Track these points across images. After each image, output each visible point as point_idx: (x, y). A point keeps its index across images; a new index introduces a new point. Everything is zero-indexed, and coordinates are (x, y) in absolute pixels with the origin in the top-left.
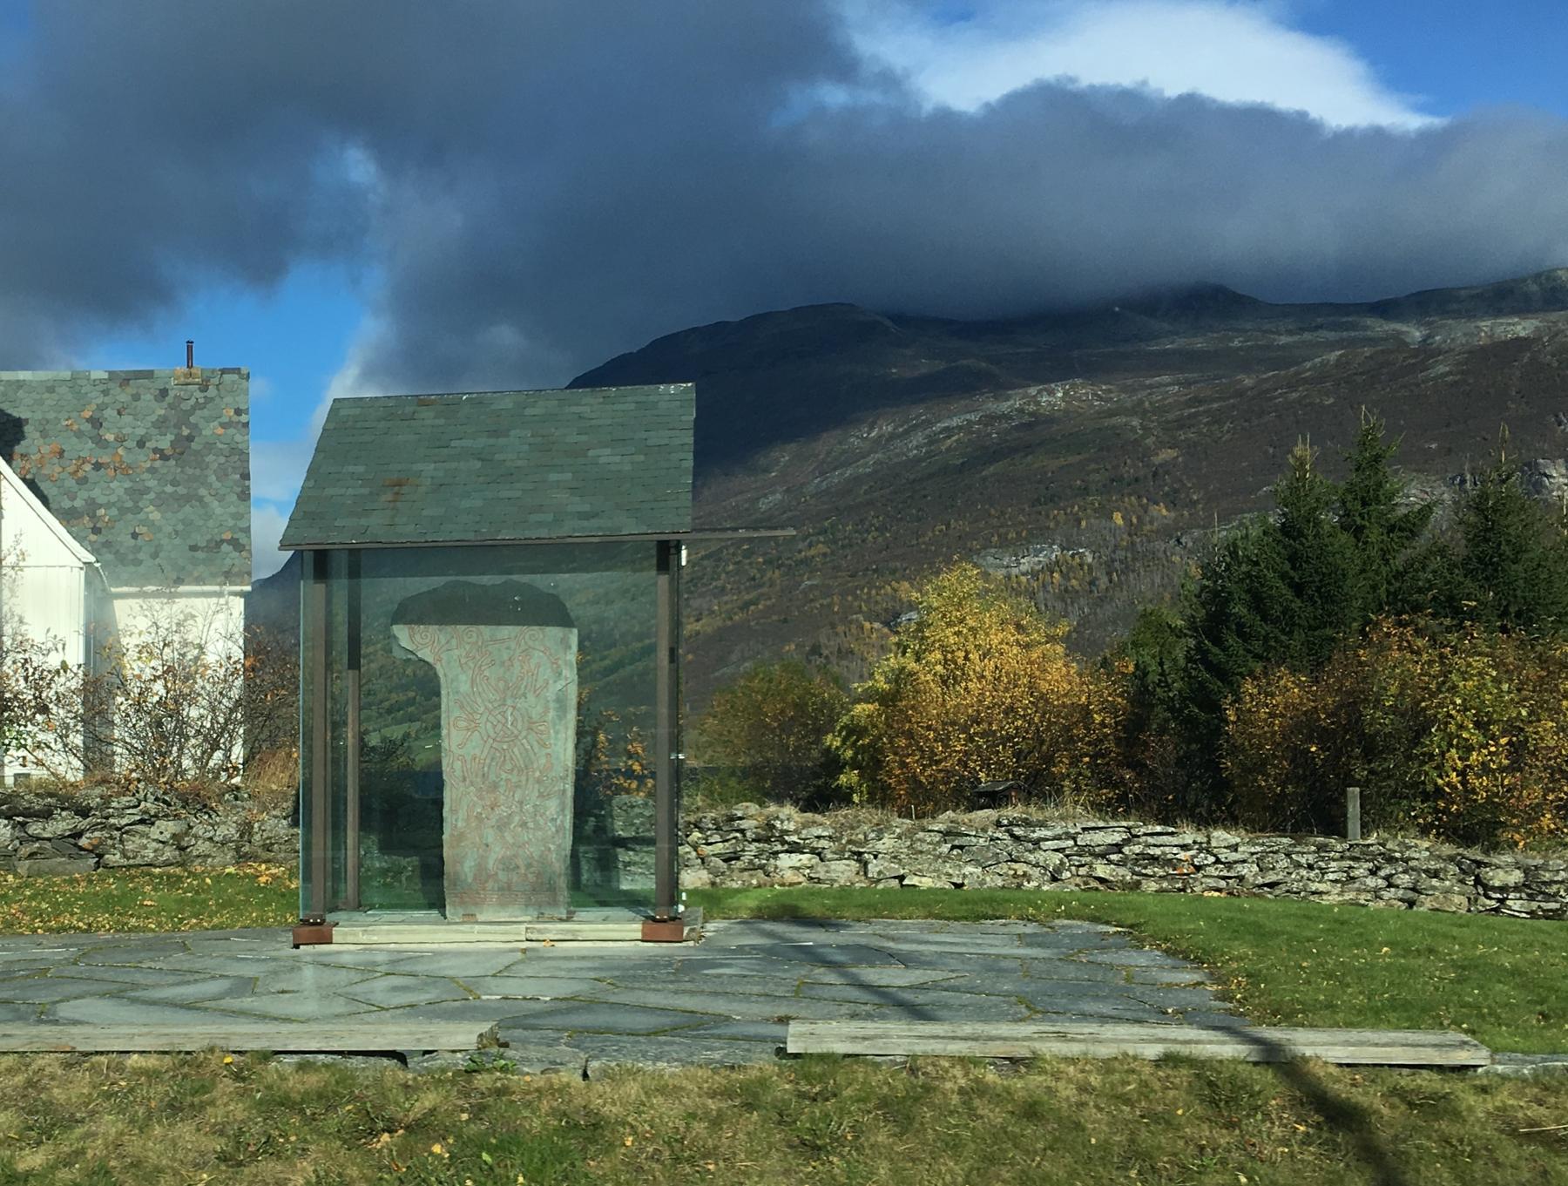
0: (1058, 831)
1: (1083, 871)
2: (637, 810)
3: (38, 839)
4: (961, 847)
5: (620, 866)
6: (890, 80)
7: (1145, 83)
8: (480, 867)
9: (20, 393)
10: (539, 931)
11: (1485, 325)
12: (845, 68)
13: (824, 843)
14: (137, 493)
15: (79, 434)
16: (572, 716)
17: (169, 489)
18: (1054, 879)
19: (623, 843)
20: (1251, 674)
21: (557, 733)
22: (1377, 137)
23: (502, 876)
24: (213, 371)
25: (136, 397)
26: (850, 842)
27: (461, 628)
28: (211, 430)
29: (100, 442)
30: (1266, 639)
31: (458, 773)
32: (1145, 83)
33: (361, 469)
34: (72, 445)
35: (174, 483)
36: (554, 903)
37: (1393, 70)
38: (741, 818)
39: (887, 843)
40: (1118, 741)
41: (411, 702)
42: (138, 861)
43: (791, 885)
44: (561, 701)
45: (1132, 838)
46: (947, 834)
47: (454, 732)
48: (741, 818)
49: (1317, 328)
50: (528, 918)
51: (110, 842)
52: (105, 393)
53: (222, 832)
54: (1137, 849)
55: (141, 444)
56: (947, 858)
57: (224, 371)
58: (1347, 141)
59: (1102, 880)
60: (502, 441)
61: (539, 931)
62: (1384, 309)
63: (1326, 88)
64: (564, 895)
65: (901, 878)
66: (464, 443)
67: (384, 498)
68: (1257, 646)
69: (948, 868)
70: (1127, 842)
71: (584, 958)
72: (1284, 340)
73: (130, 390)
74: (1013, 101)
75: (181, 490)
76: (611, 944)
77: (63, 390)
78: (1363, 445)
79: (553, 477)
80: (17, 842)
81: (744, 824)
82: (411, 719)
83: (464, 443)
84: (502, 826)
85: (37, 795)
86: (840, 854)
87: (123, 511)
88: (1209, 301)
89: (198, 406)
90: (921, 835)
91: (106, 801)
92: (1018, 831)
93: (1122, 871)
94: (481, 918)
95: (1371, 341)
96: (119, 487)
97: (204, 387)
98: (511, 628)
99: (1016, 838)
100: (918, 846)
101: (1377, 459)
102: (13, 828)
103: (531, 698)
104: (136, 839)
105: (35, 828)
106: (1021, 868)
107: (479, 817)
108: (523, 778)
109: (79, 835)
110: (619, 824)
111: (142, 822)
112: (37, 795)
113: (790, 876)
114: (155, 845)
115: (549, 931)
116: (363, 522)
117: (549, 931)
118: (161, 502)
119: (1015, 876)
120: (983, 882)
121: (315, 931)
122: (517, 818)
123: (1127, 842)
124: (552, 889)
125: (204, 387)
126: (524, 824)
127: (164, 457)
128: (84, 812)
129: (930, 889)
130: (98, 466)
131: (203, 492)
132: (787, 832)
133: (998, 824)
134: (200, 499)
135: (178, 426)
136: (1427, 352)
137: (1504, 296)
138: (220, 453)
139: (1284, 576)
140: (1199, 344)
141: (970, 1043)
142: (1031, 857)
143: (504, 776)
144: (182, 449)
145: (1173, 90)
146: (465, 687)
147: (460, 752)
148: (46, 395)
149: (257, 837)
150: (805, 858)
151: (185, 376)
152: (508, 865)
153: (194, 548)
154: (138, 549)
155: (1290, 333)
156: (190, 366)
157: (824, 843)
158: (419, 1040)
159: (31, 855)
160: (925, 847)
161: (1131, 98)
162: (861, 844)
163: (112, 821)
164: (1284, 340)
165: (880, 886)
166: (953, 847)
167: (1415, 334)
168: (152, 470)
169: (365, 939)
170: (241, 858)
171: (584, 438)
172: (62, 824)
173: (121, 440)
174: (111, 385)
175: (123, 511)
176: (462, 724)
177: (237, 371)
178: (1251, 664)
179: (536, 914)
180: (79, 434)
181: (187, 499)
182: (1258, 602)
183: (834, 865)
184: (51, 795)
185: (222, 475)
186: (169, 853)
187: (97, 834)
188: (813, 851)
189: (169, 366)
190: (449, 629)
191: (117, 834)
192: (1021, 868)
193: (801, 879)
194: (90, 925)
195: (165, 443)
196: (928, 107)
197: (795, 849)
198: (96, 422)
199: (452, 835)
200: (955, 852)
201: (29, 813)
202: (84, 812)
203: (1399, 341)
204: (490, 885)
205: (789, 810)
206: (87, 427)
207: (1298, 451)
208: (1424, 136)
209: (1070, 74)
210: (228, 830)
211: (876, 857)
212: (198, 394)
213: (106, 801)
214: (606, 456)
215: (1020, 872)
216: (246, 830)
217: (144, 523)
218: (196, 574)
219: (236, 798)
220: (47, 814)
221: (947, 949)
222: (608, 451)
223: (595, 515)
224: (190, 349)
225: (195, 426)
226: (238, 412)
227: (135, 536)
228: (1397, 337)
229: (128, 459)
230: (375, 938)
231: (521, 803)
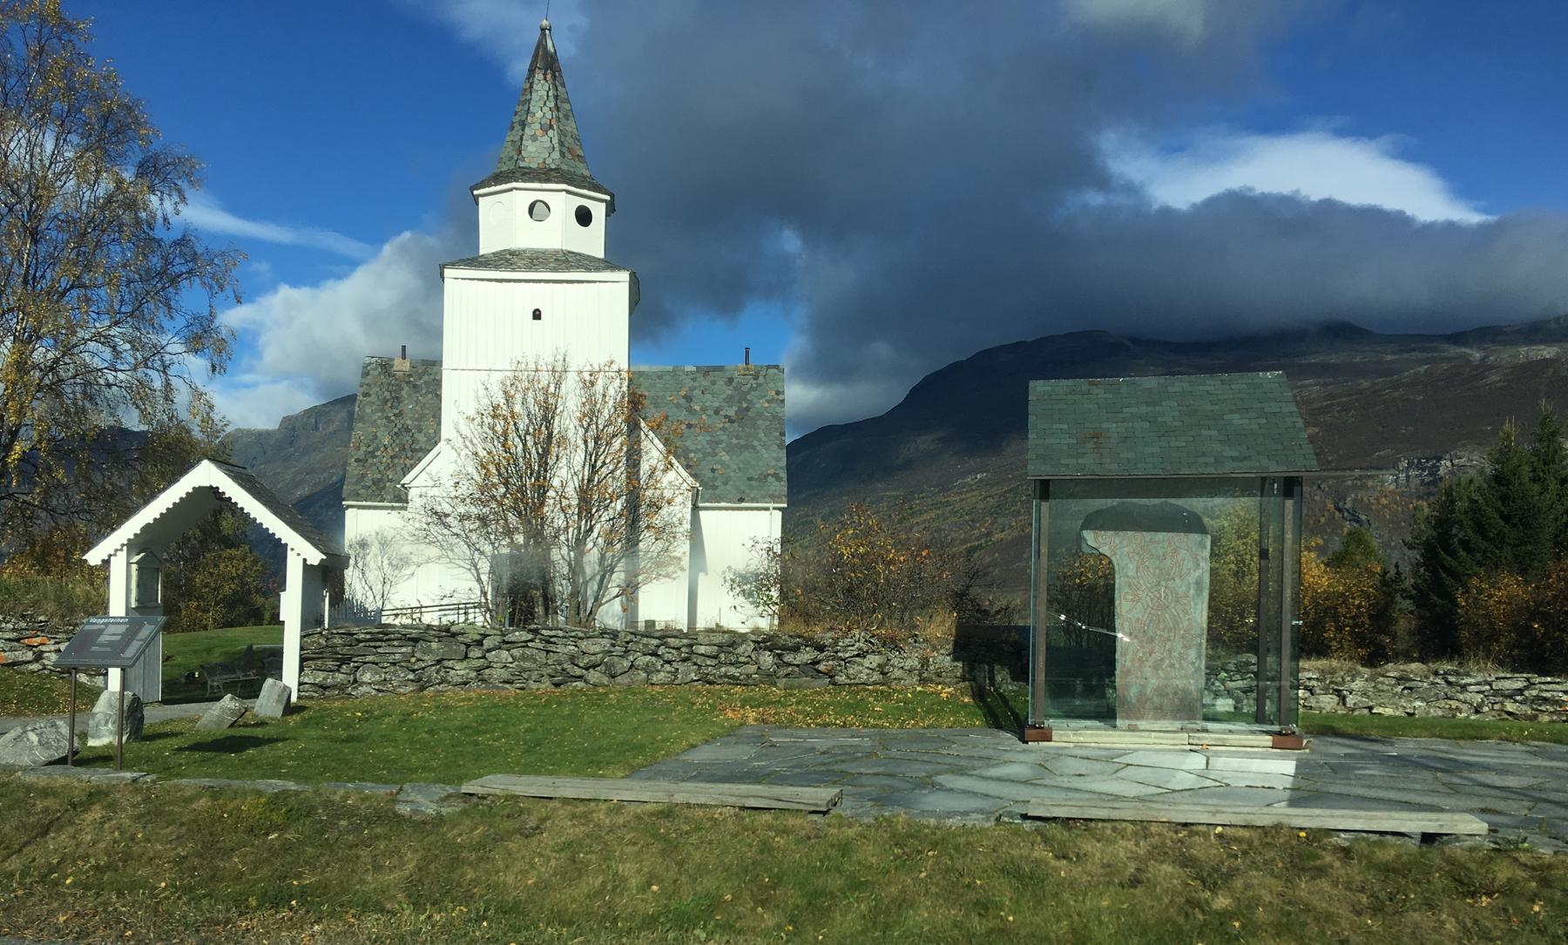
0: (1480, 679)
1: (1497, 707)
6: (1131, 189)
7: (1298, 191)
8: (1141, 694)
11: (1523, 350)
12: (1102, 181)
14: (715, 443)
15: (678, 406)
16: (1206, 594)
17: (734, 441)
18: (1477, 712)
20: (1476, 574)
22: (1450, 227)
23: (1156, 699)
25: (714, 383)
27: (1130, 533)
28: (761, 404)
29: (690, 411)
30: (1485, 552)
32: (1298, 191)
34: (673, 412)
35: (738, 437)
37: (1461, 186)
39: (1358, 684)
40: (1371, 617)
44: (1198, 583)
45: (1530, 685)
46: (1399, 680)
49: (1413, 350)
52: (694, 380)
53: (908, 664)
54: (1534, 693)
55: (717, 412)
56: (1401, 696)
57: (768, 367)
58: (1429, 229)
59: (1510, 714)
62: (1457, 338)
63: (1411, 193)
65: (1370, 708)
68: (1479, 556)
69: (1403, 702)
70: (1526, 688)
72: (1389, 358)
73: (710, 378)
74: (1213, 201)
75: (742, 442)
77: (668, 377)
78: (1543, 424)
79: (1205, 433)
83: (1135, 410)
86: (1326, 690)
87: (705, 455)
88: (1341, 331)
89: (752, 389)
91: (836, 641)
92: (1451, 679)
93: (1524, 707)
95: (1449, 360)
96: (703, 439)
97: (756, 377)
99: (1449, 683)
101: (1553, 434)
103: (1178, 581)
105: (788, 658)
106: (1454, 704)
107: (1140, 660)
109: (818, 662)
118: (730, 450)
123: (1526, 688)
125: (756, 377)
126: (1172, 666)
127: (731, 421)
128: (821, 648)
130: (689, 426)
131: (756, 443)
133: (1436, 673)
134: (754, 448)
135: (740, 402)
136: (1484, 368)
137: (1535, 331)
138: (767, 419)
139: (1497, 510)
140: (1334, 359)
142: (1461, 697)
144: (743, 414)
145: (1315, 197)
146: (1131, 573)
152: (1161, 692)
153: (750, 479)
154: (715, 479)
155: (1393, 353)
157: (1314, 683)
159: (787, 675)
161: (1289, 202)
164: (1389, 358)
167: (1477, 355)
168: (724, 429)
169: (1074, 739)
170: (923, 681)
173: (704, 410)
175: (705, 455)
177: (777, 367)
178: (1476, 569)
180: (678, 406)
181: (746, 447)
182: (1480, 528)
183: (1322, 698)
185: (768, 433)
186: (876, 677)
189: (736, 365)
192: (1454, 704)
195: (731, 412)
196: (1156, 206)
198: (688, 398)
201: (784, 648)
202: (821, 648)
203: (1466, 359)
206: (683, 401)
207: (1506, 427)
208: (1482, 227)
209: (1249, 185)
210: (913, 662)
213: (836, 641)
216: (925, 662)
217: (718, 462)
225: (750, 402)
226: (778, 393)
227: (713, 470)
228: (1464, 357)
229: (709, 422)
231: (1170, 651)
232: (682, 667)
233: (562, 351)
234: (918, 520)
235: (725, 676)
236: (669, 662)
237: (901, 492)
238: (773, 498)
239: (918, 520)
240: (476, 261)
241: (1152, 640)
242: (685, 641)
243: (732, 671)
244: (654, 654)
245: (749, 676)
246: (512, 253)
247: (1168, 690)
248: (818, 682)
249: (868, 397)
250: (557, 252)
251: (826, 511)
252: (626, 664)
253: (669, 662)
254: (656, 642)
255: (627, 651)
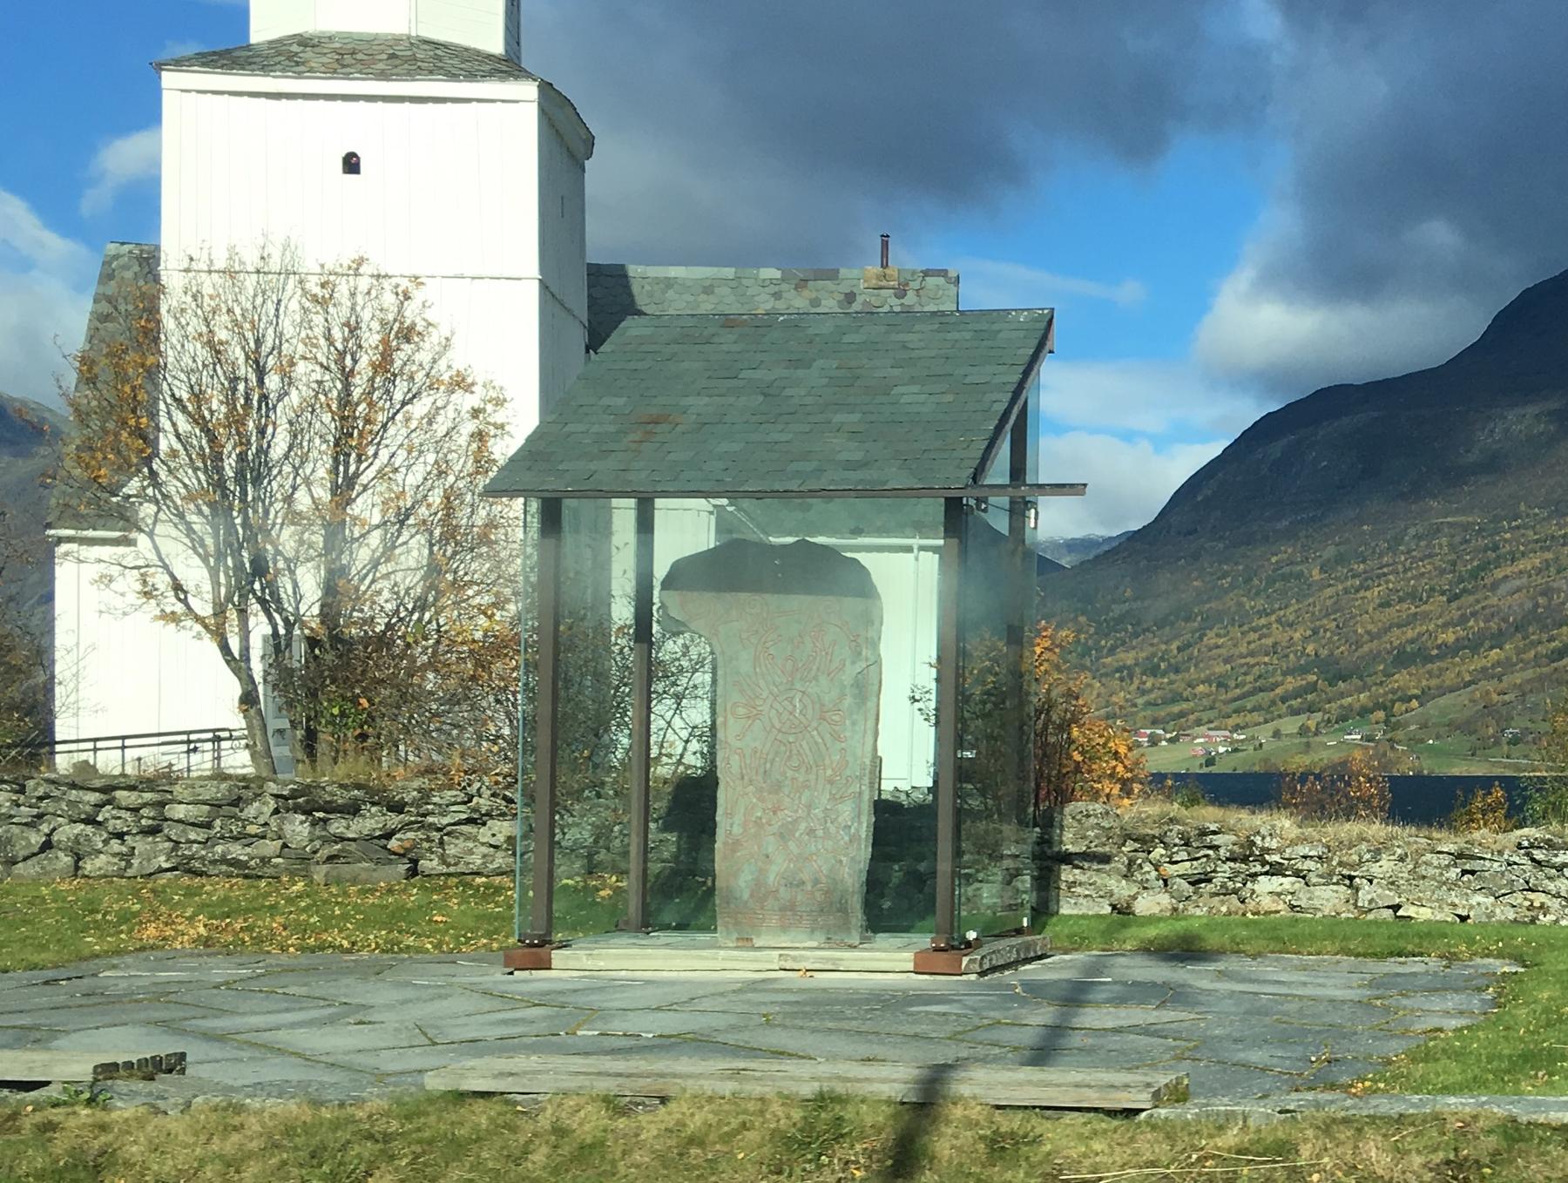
2: (1093, 820)
3: (343, 839)
4: (1473, 873)
5: (1063, 886)
8: (758, 883)
9: (670, 294)
10: (794, 959)
13: (1309, 864)
19: (1067, 858)
21: (854, 724)
24: (914, 272)
26: (1340, 864)
31: (735, 769)
33: (621, 401)
36: (845, 927)
38: (1214, 833)
41: (1312, 688)
42: (461, 868)
43: (1267, 913)
47: (731, 721)
48: (1214, 833)
50: (815, 944)
51: (426, 845)
52: (777, 296)
56: (1452, 885)
57: (926, 273)
60: (801, 373)
61: (794, 959)
64: (858, 916)
66: (758, 374)
67: (631, 437)
69: (1453, 897)
71: (789, 990)
76: (879, 976)
80: (317, 843)
81: (1218, 840)
82: (1311, 709)
83: (758, 374)
84: (784, 835)
85: (341, 786)
90: (1429, 856)
91: (425, 795)
92: (1539, 855)
94: (758, 942)
97: (901, 293)
98: (802, 597)
99: (1538, 863)
100: (1422, 870)
102: (313, 824)
103: (823, 680)
104: (460, 842)
105: (337, 826)
107: (758, 823)
108: (812, 777)
109: (389, 835)
110: (1068, 836)
111: (469, 821)
112: (341, 786)
113: (1267, 903)
114: (485, 850)
115: (806, 959)
116: (593, 466)
117: (806, 959)
119: (1531, 908)
120: (1491, 915)
121: (535, 951)
122: (803, 826)
124: (843, 909)
125: (901, 293)
128: (398, 808)
129: (1428, 922)
132: (1268, 851)
141: (620, 1080)
143: (790, 773)
147: (739, 744)
148: (703, 297)
149: (617, 843)
150: (1287, 882)
151: (878, 278)
156: (885, 265)
158: (30, 1069)
159: (331, 859)
160: (1431, 872)
162: (1352, 866)
163: (430, 819)
165: (1370, 917)
166: (1464, 872)
169: (589, 964)
171: (897, 372)
172: (371, 821)
174: (785, 286)
176: (741, 711)
177: (943, 273)
179: (823, 939)
183: (1318, 891)
184: (358, 787)
187: (410, 835)
188: (1298, 874)
190: (728, 596)
191: (436, 835)
192: (1538, 899)
193: (1281, 906)
194: (353, 944)
197: (1276, 870)
199: (725, 844)
200: (1465, 878)
201: (330, 808)
204: (770, 903)
205: (1286, 824)
211: (1371, 881)
212: (894, 301)
213: (425, 795)
214: (910, 396)
215: (1537, 904)
218: (879, 524)
219: (599, 796)
220: (353, 810)
221: (1284, 990)
222: (915, 388)
223: (864, 464)
224: (885, 245)
230: (602, 964)
231: (809, 807)
232: (141, 845)
233: (206, 245)
234: (1508, 571)
235: (224, 860)
236: (120, 836)
237: (1475, 518)
238: (920, 528)
239: (1508, 571)
240: (233, 55)
241: (777, 788)
242: (148, 796)
243: (237, 851)
244: (90, 821)
245: (265, 861)
246: (304, 41)
247: (805, 876)
248: (388, 870)
249: (1413, 328)
250: (397, 40)
251: (1330, 552)
252: (36, 839)
253: (120, 836)
254: (93, 797)
255: (40, 816)
